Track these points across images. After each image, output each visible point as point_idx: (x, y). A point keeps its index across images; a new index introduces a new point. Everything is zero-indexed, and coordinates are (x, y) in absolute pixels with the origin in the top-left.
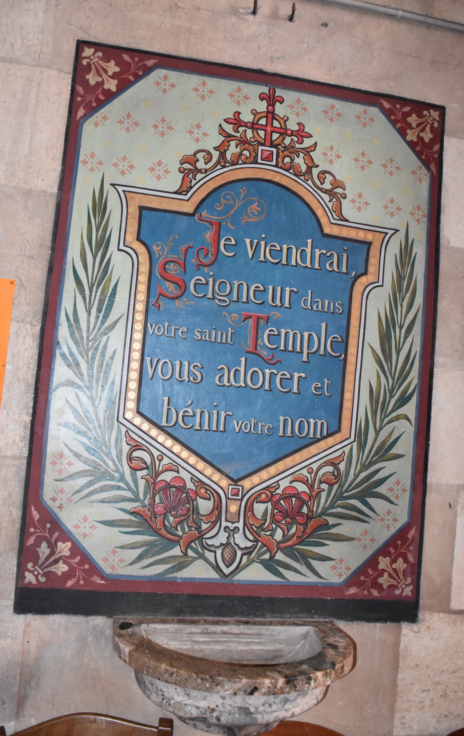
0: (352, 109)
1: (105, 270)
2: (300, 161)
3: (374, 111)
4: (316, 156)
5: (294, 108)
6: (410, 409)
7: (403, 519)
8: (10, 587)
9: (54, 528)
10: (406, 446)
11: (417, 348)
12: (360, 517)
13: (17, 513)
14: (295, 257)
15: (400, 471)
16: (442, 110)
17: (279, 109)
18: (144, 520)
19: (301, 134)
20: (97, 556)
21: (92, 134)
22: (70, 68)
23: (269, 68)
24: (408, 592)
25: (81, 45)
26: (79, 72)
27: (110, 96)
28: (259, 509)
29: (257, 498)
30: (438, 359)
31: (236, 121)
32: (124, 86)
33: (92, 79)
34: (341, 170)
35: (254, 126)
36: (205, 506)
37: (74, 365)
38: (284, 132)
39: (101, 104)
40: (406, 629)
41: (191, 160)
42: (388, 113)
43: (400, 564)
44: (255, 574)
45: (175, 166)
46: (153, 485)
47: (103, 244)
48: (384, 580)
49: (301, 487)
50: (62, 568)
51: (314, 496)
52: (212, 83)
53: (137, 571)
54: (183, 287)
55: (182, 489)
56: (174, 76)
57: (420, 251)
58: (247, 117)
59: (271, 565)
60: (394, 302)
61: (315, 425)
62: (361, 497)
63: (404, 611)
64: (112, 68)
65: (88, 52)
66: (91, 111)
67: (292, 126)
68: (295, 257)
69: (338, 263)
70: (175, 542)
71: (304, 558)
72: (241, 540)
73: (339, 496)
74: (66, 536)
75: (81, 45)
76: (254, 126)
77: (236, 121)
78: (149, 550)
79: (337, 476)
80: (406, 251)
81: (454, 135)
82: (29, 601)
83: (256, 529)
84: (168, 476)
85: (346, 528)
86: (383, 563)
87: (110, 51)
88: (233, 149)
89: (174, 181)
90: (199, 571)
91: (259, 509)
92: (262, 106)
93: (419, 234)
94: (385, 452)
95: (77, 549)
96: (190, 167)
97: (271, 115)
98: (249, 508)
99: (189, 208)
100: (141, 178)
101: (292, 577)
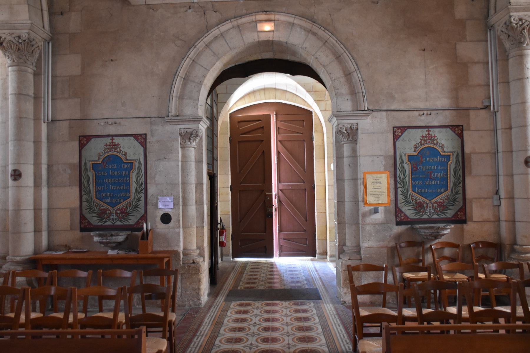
0: (444, 130)
1: (404, 167)
2: (435, 142)
3: (448, 129)
4: (438, 140)
5: (433, 132)
6: (461, 185)
7: (462, 205)
8: (395, 221)
9: (401, 212)
10: (461, 192)
11: (461, 173)
12: (453, 205)
13: (394, 209)
14: (436, 160)
15: (460, 196)
16: (462, 126)
17: (430, 133)
18: (415, 209)
19: (435, 137)
20: (408, 215)
21: (398, 143)
22: (392, 132)
23: (428, 125)
24: (464, 218)
25: (394, 127)
26: (394, 133)
27: (400, 136)
28: (435, 205)
29: (434, 203)
30: (466, 175)
31: (423, 137)
32: (402, 134)
33: (396, 133)
34: (443, 142)
35: (426, 137)
36: (425, 205)
37: (400, 184)
38: (432, 137)
39: (399, 138)
40: (465, 226)
41: (415, 145)
42: (451, 129)
43: (462, 213)
44: (435, 216)
45: (412, 146)
46: (416, 203)
47: (403, 163)
48: (459, 216)
49: (442, 201)
50: (403, 218)
51: (444, 202)
52: (417, 130)
53: (415, 217)
54: (417, 168)
55: (421, 203)
56: (410, 130)
57: (460, 155)
58: (425, 135)
59: (438, 215)
60: (456, 166)
61: (443, 190)
62: (453, 201)
63: (464, 222)
64: (399, 131)
65: (395, 129)
66: (397, 139)
67: (433, 135)
68: (436, 160)
69: (444, 160)
70: (420, 212)
71: (444, 213)
72: (432, 211)
73: (449, 202)
74: (403, 212)
75: (394, 127)
76: (426, 137)
77: (423, 137)
78: (417, 214)
79: (448, 198)
80: (457, 155)
81: (466, 130)
82: (398, 224)
83: (435, 209)
84: (418, 201)
85: (451, 207)
86: (459, 213)
87: (399, 128)
88: (423, 142)
89: (413, 150)
90: (425, 217)
91: (435, 205)
92: (427, 133)
93: (460, 152)
94: (457, 193)
95: (405, 214)
96: (415, 147)
97: (429, 134)
98: (433, 205)
99: (416, 154)
100: (407, 150)
101: (442, 216)
